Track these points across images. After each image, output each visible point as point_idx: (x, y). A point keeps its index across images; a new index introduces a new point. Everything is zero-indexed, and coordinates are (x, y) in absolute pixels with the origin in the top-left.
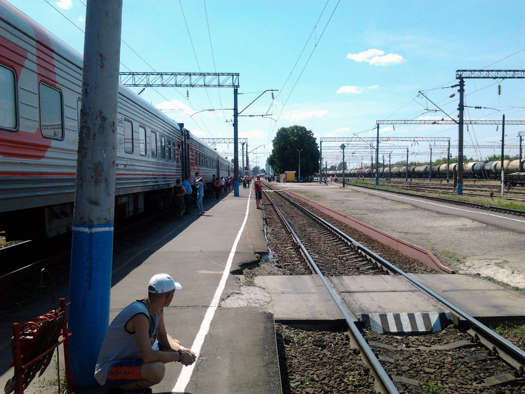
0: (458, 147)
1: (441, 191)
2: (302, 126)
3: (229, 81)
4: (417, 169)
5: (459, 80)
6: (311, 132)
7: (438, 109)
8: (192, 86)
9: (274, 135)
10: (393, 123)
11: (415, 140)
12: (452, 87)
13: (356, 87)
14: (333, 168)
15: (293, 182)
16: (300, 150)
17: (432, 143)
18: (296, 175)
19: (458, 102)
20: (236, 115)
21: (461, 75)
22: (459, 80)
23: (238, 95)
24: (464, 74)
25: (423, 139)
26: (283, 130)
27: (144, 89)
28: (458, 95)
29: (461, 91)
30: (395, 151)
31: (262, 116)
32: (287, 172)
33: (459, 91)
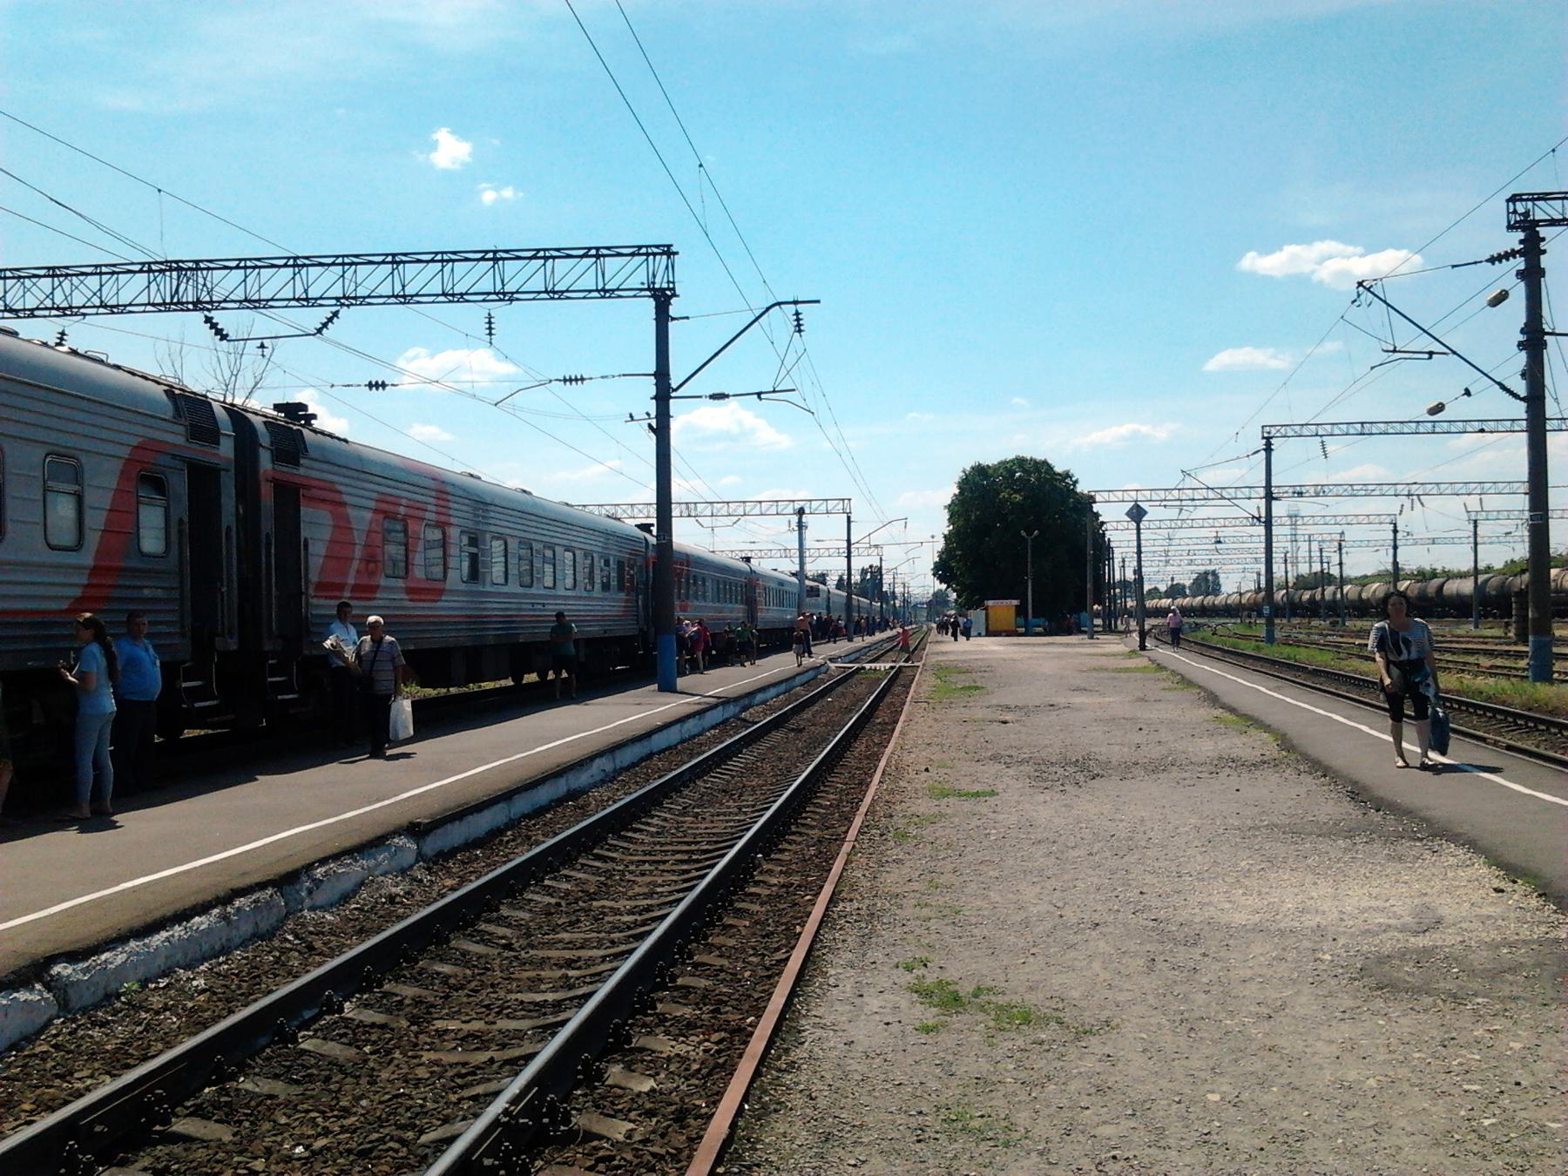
0: (1525, 488)
1: (1485, 662)
2: (1039, 457)
3: (634, 273)
4: (1452, 587)
5: (1521, 235)
6: (1067, 475)
7: (1437, 347)
8: (507, 297)
9: (949, 491)
10: (1320, 432)
11: (1413, 494)
12: (1492, 260)
13: (1271, 351)
14: (1175, 591)
15: (1009, 634)
16: (1030, 533)
17: (1473, 503)
18: (1021, 611)
19: (1521, 319)
20: (663, 396)
21: (1527, 214)
22: (1521, 235)
23: (671, 324)
24: (1541, 211)
25: (1439, 488)
26: (980, 471)
27: (335, 314)
28: (1519, 292)
29: (1533, 276)
30: (1351, 534)
31: (759, 394)
32: (990, 603)
33: (1520, 274)
